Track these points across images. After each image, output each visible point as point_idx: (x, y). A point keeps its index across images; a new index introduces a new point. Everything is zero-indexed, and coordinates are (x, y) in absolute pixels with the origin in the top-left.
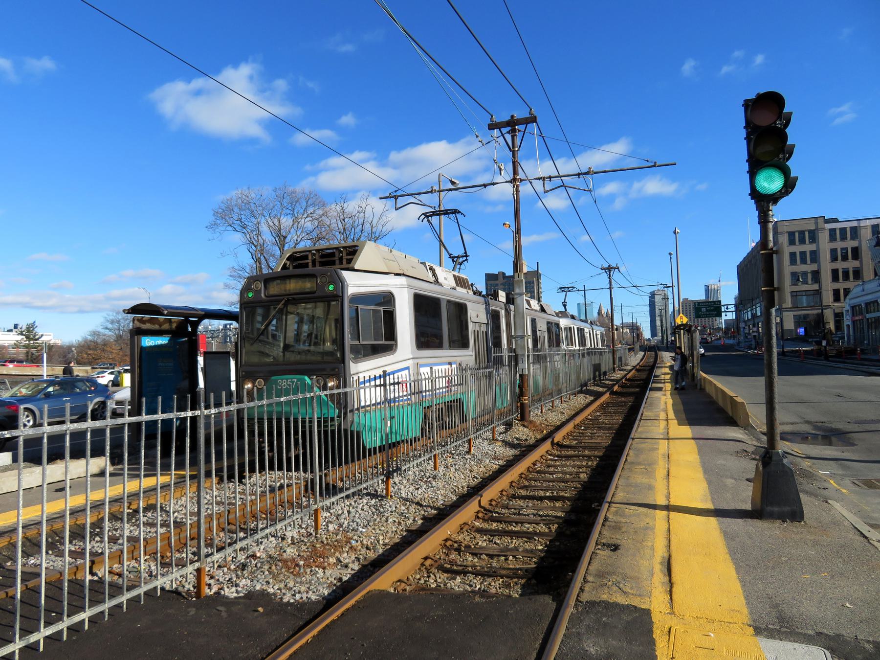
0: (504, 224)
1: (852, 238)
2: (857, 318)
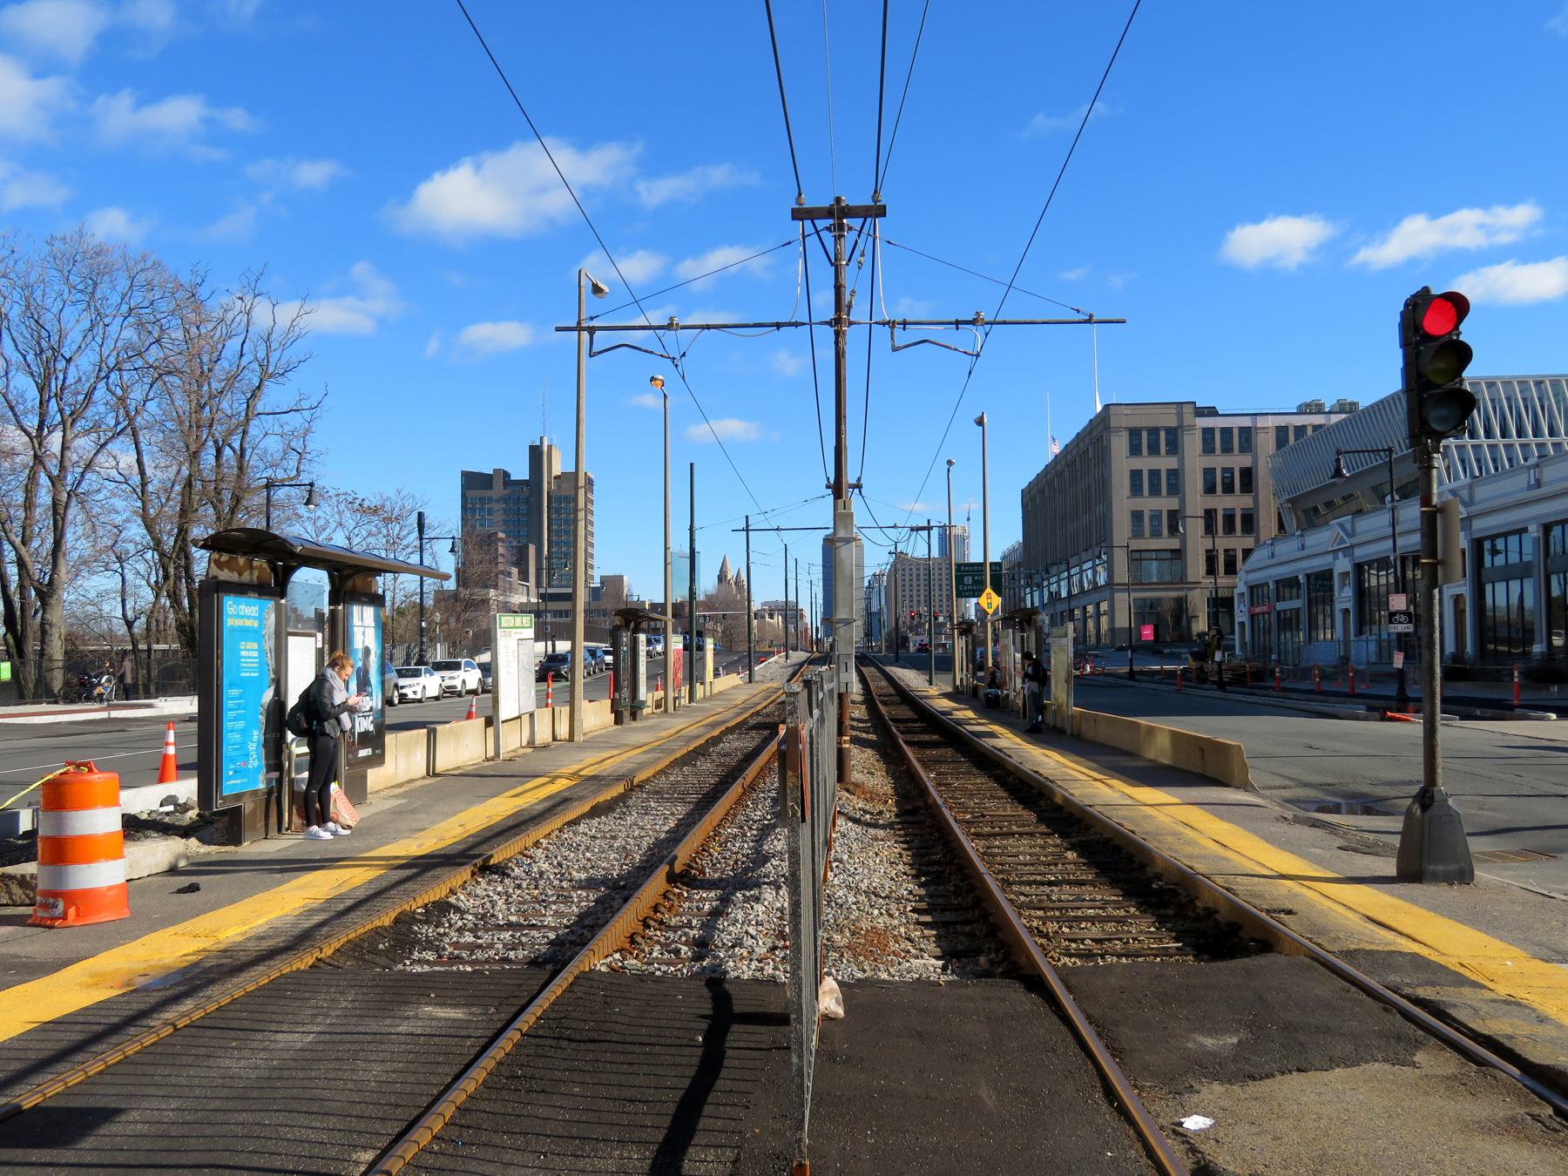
0: (653, 379)
1: (1243, 450)
2: (1258, 610)
